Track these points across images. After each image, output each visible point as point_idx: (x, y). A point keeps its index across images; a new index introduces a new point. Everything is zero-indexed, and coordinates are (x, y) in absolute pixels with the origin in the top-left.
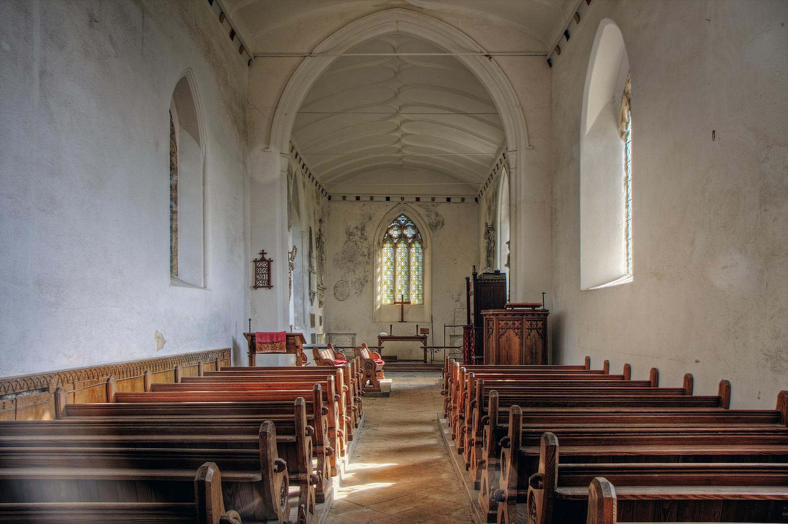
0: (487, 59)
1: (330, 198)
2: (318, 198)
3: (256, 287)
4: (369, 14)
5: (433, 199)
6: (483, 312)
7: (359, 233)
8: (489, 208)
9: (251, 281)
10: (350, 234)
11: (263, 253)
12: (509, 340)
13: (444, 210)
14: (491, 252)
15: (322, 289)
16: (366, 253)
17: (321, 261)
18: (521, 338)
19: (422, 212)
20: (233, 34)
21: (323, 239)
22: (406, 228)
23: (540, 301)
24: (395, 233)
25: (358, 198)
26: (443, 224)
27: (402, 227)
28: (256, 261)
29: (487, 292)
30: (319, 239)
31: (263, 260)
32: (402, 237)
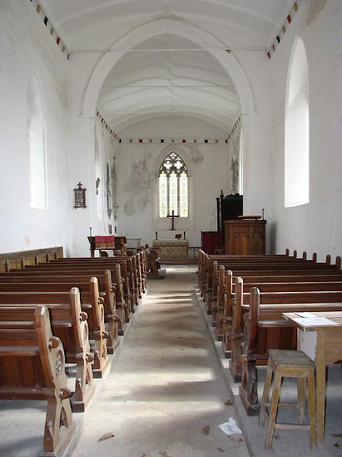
0: (227, 52)
1: (120, 141)
2: (112, 142)
3: (76, 207)
4: (148, 22)
5: (195, 141)
6: (225, 222)
7: (142, 166)
8: (234, 148)
9: (73, 204)
10: (135, 167)
11: (80, 185)
12: (240, 240)
13: (203, 149)
14: (235, 179)
15: (116, 207)
16: (147, 180)
17: (115, 186)
18: (248, 238)
19: (187, 150)
20: (46, 20)
21: (116, 171)
22: (176, 162)
23: (261, 214)
24: (168, 166)
25: (141, 141)
26: (202, 159)
27: (173, 162)
28: (75, 190)
29: (230, 206)
30: (113, 172)
31: (80, 189)
32: (173, 168)
